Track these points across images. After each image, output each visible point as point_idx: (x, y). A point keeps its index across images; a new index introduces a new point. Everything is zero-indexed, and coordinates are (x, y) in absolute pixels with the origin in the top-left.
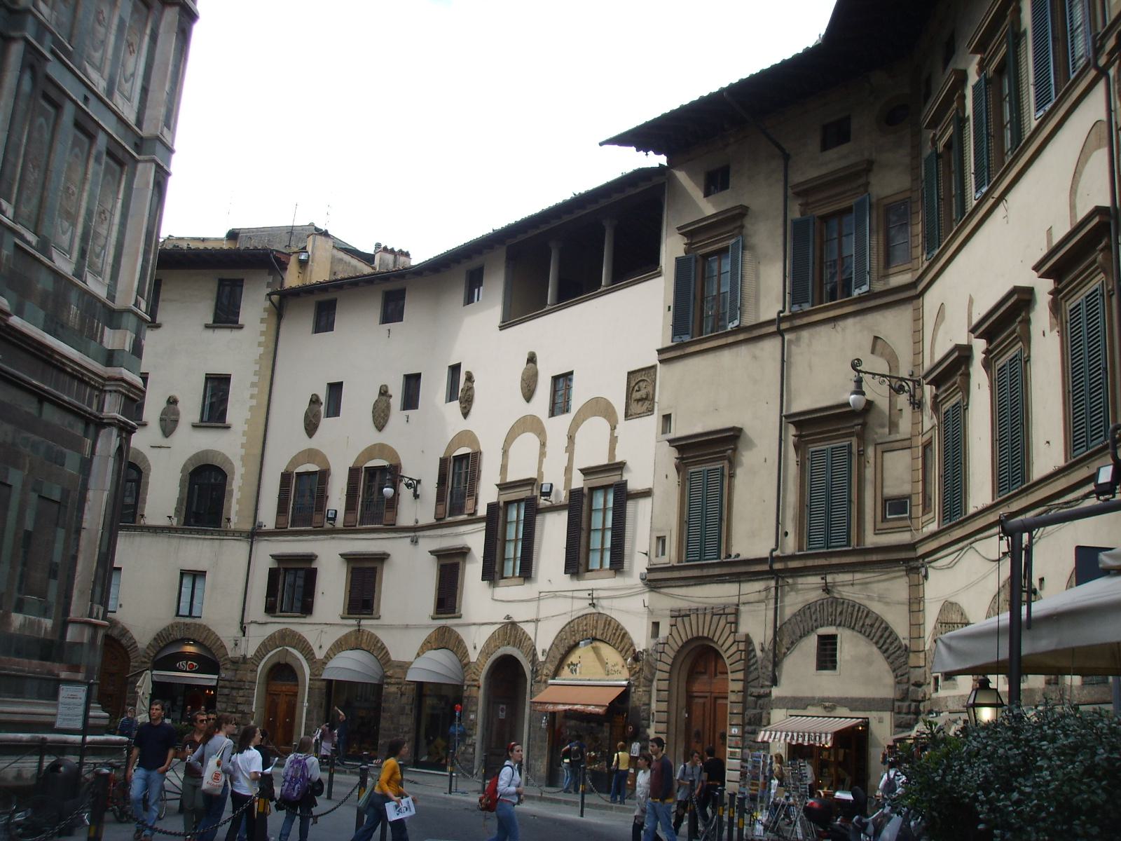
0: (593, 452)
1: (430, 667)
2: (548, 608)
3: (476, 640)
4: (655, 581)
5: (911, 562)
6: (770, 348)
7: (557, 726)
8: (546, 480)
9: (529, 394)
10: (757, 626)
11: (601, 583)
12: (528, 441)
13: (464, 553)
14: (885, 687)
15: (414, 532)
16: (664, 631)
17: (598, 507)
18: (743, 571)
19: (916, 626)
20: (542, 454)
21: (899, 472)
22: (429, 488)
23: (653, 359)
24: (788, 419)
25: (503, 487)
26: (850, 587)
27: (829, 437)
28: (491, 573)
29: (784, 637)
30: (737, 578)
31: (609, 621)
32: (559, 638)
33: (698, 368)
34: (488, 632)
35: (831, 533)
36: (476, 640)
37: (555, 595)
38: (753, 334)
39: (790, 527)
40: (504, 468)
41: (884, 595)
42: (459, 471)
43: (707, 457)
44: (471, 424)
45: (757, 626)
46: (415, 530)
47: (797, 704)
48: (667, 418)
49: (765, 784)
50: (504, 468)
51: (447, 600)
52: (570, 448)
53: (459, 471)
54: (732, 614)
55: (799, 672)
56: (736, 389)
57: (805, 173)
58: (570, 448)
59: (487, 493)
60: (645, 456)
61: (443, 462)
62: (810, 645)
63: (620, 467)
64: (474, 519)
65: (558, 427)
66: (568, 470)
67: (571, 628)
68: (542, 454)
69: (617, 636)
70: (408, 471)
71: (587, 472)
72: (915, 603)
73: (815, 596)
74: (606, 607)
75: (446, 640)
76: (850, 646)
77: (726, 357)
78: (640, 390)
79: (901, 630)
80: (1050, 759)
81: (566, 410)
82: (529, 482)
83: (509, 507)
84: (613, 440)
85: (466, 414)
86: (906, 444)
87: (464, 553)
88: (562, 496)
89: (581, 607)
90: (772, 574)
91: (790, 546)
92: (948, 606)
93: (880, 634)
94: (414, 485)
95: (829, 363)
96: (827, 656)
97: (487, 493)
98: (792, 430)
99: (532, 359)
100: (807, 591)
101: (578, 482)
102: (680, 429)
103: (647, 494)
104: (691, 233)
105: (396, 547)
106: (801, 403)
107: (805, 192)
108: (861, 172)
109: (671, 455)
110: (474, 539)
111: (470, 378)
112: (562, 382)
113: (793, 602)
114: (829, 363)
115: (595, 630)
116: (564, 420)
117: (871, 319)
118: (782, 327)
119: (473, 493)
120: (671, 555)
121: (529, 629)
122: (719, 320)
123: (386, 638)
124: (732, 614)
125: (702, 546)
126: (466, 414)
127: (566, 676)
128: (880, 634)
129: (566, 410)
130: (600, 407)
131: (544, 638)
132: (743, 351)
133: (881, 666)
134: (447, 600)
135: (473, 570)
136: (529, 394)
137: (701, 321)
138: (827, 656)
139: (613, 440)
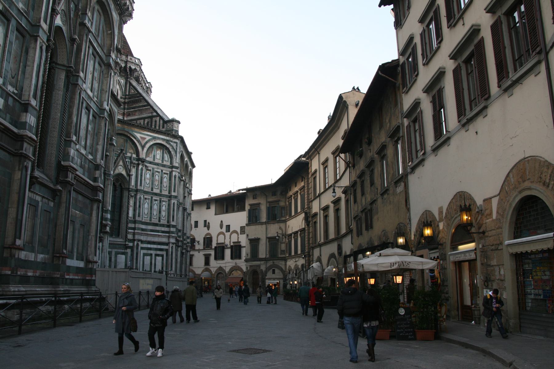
0: (234, 238)
1: (206, 275)
2: (227, 265)
3: (213, 270)
4: (246, 261)
5: (285, 259)
6: (264, 226)
7: (106, 62)
8: (226, 243)
9: (221, 227)
10: (263, 268)
11: (238, 261)
12: (221, 236)
13: (210, 255)
14: (282, 276)
15: (113, 205)
16: (249, 269)
17: (236, 250)
18: (261, 260)
19: (286, 268)
20: (225, 239)
21: (283, 247)
22: (202, 242)
23: (245, 225)
24: (267, 238)
25: (217, 244)
26: (276, 262)
27: (273, 241)
28: (216, 259)
29: (268, 269)
30: (155, 165)
31: (239, 267)
32: (230, 269)
33: (253, 227)
34: (216, 269)
35: (274, 253)
36: (213, 270)
37: (229, 262)
38: (262, 224)
39: (268, 253)
40: (217, 240)
41: (281, 264)
42: (208, 241)
43: (254, 243)
44: (210, 232)
45: (263, 268)
46: (199, 250)
47: (270, 279)
48: (248, 235)
49: (309, 252)
50: (217, 240)
51: (207, 262)
52: (230, 238)
53: (208, 241)
54: (259, 266)
55: (270, 274)
56: (258, 231)
57: (270, 200)
58: (230, 238)
59: (214, 245)
60: (243, 240)
61: (204, 238)
62: (271, 270)
63: (240, 242)
64: (211, 249)
65: (227, 234)
66: (230, 242)
67: (232, 268)
68: (225, 239)
69: (241, 269)
70: (197, 239)
71: (234, 243)
72: (286, 265)
73: (272, 264)
74: (238, 264)
75: (207, 270)
76: (277, 271)
77: (257, 226)
78: (243, 229)
79: (284, 269)
80: (269, 298)
81: (229, 231)
82: (223, 243)
83: (166, 119)
84: (238, 238)
85: (208, 230)
86: (284, 243)
87: (210, 255)
88: (229, 246)
89: (234, 264)
90: (265, 260)
91: (268, 256)
92: (290, 266)
93: (281, 269)
94: (198, 242)
95: (274, 230)
96: (274, 272)
97: (214, 245)
98: (268, 240)
99: (222, 222)
100: (270, 263)
101: (232, 244)
102: (250, 237)
103: (245, 247)
104: (251, 205)
105: (196, 253)
106: (269, 236)
107: (270, 202)
108: (278, 201)
109: (248, 242)
110: (212, 253)
111: (209, 223)
112: (228, 227)
113: (268, 265)
114: (274, 230)
115: (236, 268)
116: (229, 233)
117: (279, 224)
118: (265, 223)
119: (211, 244)
120: (249, 257)
121: (224, 268)
122: (256, 221)
123: (195, 270)
124: (259, 266)
125: (254, 254)
126: (208, 230)
127: (231, 276)
128: (281, 269)
129: (229, 231)
130: (235, 232)
131: (227, 270)
132: (260, 226)
133: (281, 273)
134: (207, 262)
135: (212, 258)
136: (221, 227)
137: (253, 219)
138: (274, 272)
139: (238, 238)
